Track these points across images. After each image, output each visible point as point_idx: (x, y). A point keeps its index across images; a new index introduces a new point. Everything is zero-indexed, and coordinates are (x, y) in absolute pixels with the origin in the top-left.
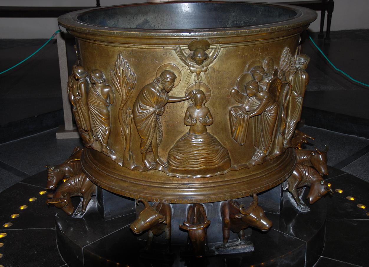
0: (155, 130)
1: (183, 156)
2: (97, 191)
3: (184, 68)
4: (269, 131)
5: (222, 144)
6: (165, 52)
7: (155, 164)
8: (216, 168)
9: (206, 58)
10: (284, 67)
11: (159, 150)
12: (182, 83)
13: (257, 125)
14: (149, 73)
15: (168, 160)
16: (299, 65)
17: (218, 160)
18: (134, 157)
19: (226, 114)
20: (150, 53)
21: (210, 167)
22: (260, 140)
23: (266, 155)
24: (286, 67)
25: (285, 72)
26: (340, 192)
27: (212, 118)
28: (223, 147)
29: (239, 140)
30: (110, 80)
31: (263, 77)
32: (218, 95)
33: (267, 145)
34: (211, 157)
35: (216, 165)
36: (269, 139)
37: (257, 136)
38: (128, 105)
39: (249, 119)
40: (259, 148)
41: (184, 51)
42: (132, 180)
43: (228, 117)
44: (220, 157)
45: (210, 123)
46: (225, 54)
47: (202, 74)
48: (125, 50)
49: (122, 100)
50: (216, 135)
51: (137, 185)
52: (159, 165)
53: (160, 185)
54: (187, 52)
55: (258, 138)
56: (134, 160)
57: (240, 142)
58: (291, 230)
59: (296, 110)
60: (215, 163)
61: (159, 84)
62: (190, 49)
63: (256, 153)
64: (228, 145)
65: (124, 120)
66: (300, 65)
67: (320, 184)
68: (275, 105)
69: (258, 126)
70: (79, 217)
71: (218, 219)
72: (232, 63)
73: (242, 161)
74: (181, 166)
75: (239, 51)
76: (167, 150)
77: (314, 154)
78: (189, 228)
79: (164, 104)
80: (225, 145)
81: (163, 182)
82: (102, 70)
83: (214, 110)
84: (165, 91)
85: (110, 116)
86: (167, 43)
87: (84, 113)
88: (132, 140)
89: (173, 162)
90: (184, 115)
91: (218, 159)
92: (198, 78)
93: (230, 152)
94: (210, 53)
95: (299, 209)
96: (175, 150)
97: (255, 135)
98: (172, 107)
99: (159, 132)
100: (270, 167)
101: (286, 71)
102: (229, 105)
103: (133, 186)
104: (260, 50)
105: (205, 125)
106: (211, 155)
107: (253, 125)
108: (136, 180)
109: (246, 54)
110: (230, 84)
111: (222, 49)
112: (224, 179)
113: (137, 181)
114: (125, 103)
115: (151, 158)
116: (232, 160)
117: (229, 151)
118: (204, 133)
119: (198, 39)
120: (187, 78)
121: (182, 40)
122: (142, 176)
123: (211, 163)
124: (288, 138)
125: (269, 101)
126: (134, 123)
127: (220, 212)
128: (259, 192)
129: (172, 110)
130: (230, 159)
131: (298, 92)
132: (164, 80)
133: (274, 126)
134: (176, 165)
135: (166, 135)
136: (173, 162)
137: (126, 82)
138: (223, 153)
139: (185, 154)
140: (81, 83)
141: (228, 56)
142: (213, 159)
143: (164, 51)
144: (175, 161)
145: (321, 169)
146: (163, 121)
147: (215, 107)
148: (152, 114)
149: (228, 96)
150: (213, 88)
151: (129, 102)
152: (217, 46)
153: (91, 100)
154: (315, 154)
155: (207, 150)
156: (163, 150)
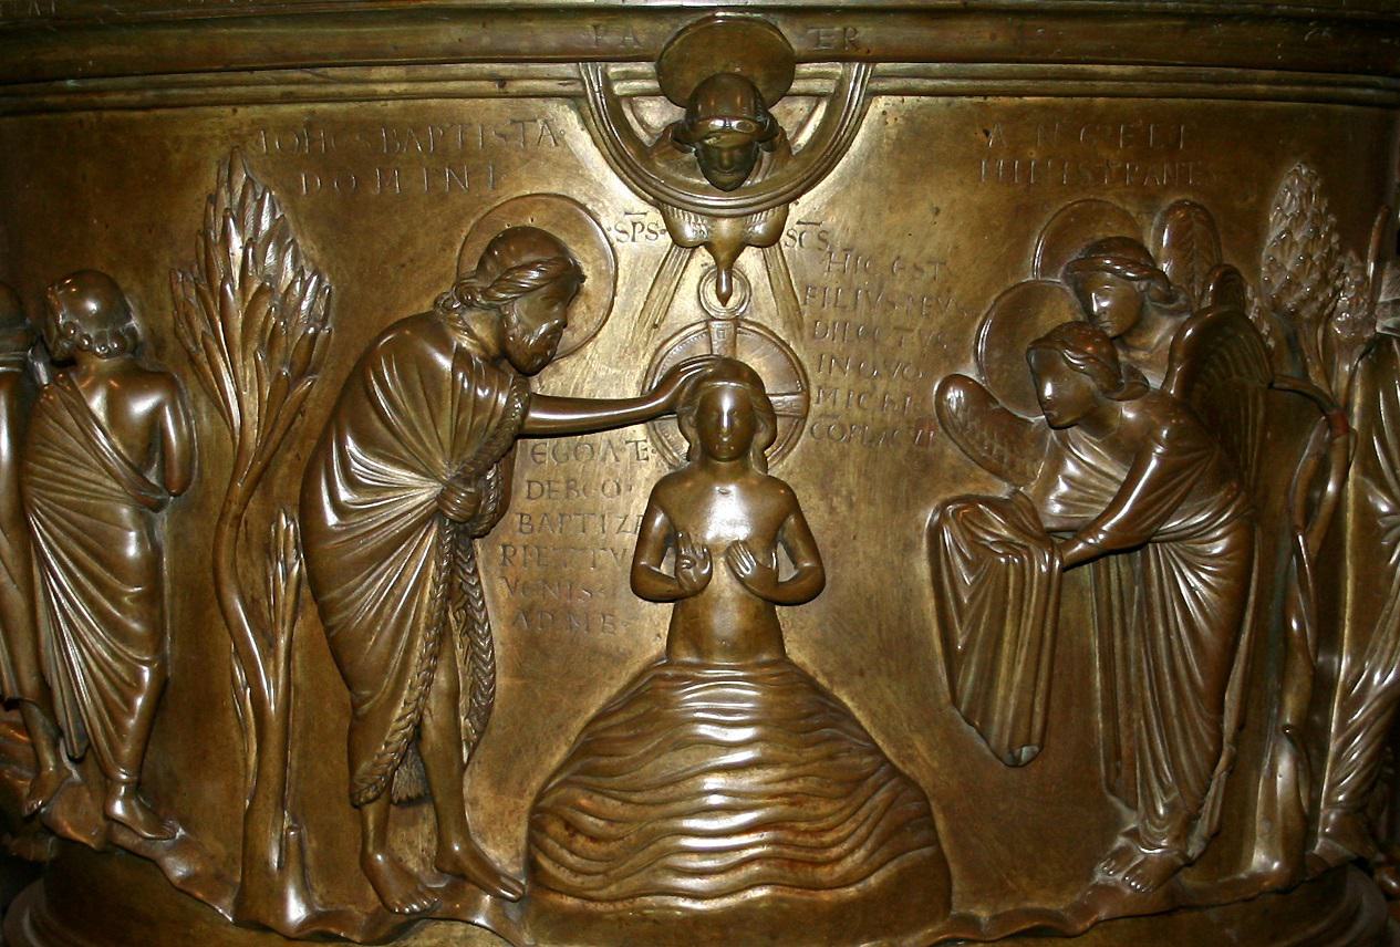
0: (443, 636)
3: (634, 224)
5: (888, 752)
8: (850, 904)
9: (770, 136)
10: (1291, 285)
11: (475, 787)
12: (620, 327)
13: (1118, 642)
15: (529, 853)
17: (860, 854)
18: (312, 845)
19: (909, 547)
20: (417, 129)
21: (806, 898)
23: (1183, 854)
24: (1299, 285)
25: (1293, 315)
28: (894, 772)
30: (169, 337)
32: (857, 413)
33: (1191, 780)
34: (808, 820)
35: (847, 886)
37: (1122, 720)
38: (276, 490)
39: (1061, 579)
40: (1140, 804)
43: (923, 568)
44: (870, 833)
46: (899, 144)
48: (259, 125)
52: (470, 887)
55: (1128, 738)
56: (312, 873)
57: (1006, 741)
59: (1389, 605)
60: (839, 869)
61: (468, 316)
63: (1121, 841)
64: (924, 761)
65: (253, 600)
68: (1234, 499)
69: (1125, 648)
72: (943, 206)
73: (1024, 881)
74: (613, 888)
76: (521, 784)
80: (911, 759)
82: (126, 281)
83: (832, 510)
84: (517, 363)
85: (167, 588)
86: (524, 45)
88: (297, 728)
89: (559, 862)
90: (630, 539)
91: (858, 846)
92: (724, 289)
94: (801, 127)
97: (1110, 712)
99: (473, 655)
104: (1125, 146)
105: (767, 597)
106: (807, 810)
107: (1095, 643)
109: (1033, 155)
110: (937, 343)
111: (881, 103)
114: (256, 469)
115: (421, 843)
116: (954, 869)
117: (933, 804)
118: (765, 657)
119: (720, 14)
121: (619, 26)
123: (815, 864)
129: (559, 506)
130: (940, 860)
132: (500, 279)
135: (519, 682)
136: (559, 862)
137: (263, 330)
139: (636, 797)
141: (914, 152)
142: (828, 838)
144: (572, 852)
145: (1360, 408)
147: (837, 493)
148: (423, 522)
149: (920, 424)
150: (825, 365)
151: (284, 470)
152: (842, 83)
153: (47, 465)
156: (499, 784)
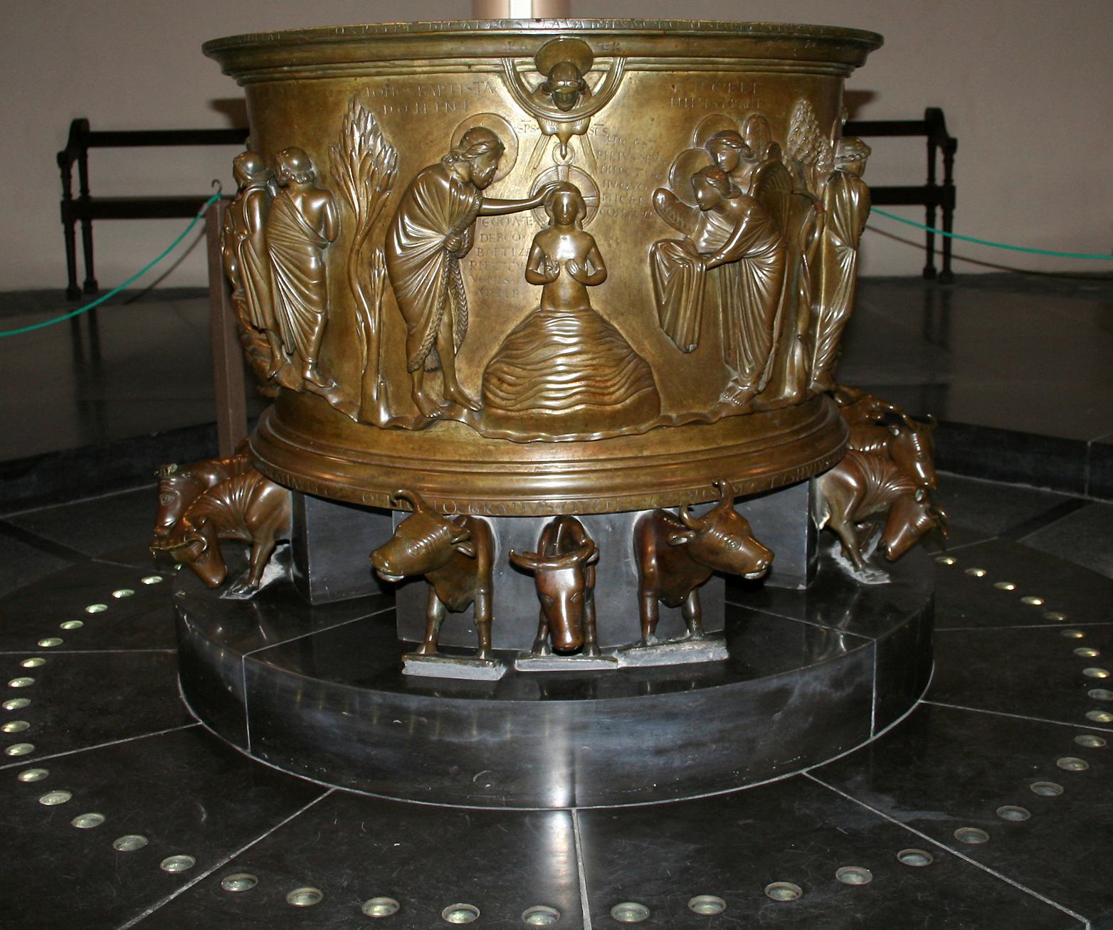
0: (446, 301)
1: (524, 373)
2: (291, 525)
4: (763, 316)
5: (634, 347)
6: (474, 83)
7: (446, 405)
8: (618, 412)
9: (583, 88)
10: (800, 150)
11: (459, 363)
12: (520, 169)
13: (729, 300)
14: (431, 142)
16: (842, 162)
17: (623, 390)
18: (390, 389)
19: (642, 261)
22: (739, 347)
26: (980, 574)
27: (604, 265)
28: (636, 356)
29: (681, 335)
30: (328, 174)
31: (739, 159)
32: (619, 205)
34: (601, 376)
36: (763, 340)
37: (731, 332)
38: (374, 239)
39: (706, 274)
41: (525, 77)
42: (385, 459)
43: (648, 270)
45: (599, 276)
46: (637, 92)
47: (574, 140)
49: (359, 222)
50: (616, 318)
51: (397, 470)
53: (460, 467)
54: (535, 79)
58: (842, 644)
60: (614, 397)
62: (539, 69)
63: (731, 384)
64: (649, 351)
66: (845, 164)
67: (914, 502)
69: (732, 303)
70: (241, 598)
71: (627, 573)
72: (655, 117)
73: (691, 401)
75: (673, 87)
77: (897, 432)
78: (535, 564)
79: (471, 218)
81: (469, 459)
82: (309, 151)
83: (610, 246)
84: (477, 185)
87: (258, 278)
88: (384, 338)
90: (525, 258)
92: (564, 153)
93: (658, 371)
94: (596, 84)
95: (859, 579)
96: (504, 357)
98: (492, 236)
99: (459, 308)
100: (770, 434)
101: (806, 162)
102: (649, 234)
103: (387, 474)
105: (583, 282)
106: (601, 371)
108: (393, 460)
109: (693, 96)
110: (653, 175)
111: (629, 74)
112: (641, 451)
113: (398, 460)
115: (437, 388)
116: (661, 396)
117: (653, 369)
119: (562, 37)
120: (533, 151)
122: (411, 446)
123: (603, 395)
124: (821, 365)
125: (758, 223)
126: (390, 289)
127: (630, 550)
128: (741, 494)
130: (655, 392)
131: (841, 232)
133: (776, 303)
134: (504, 402)
137: (369, 172)
138: (635, 369)
139: (528, 367)
140: (250, 196)
141: (643, 95)
143: (472, 79)
144: (501, 391)
146: (470, 279)
147: (612, 239)
151: (377, 231)
152: (613, 66)
154: (900, 433)
155: (590, 356)
156: (470, 361)
